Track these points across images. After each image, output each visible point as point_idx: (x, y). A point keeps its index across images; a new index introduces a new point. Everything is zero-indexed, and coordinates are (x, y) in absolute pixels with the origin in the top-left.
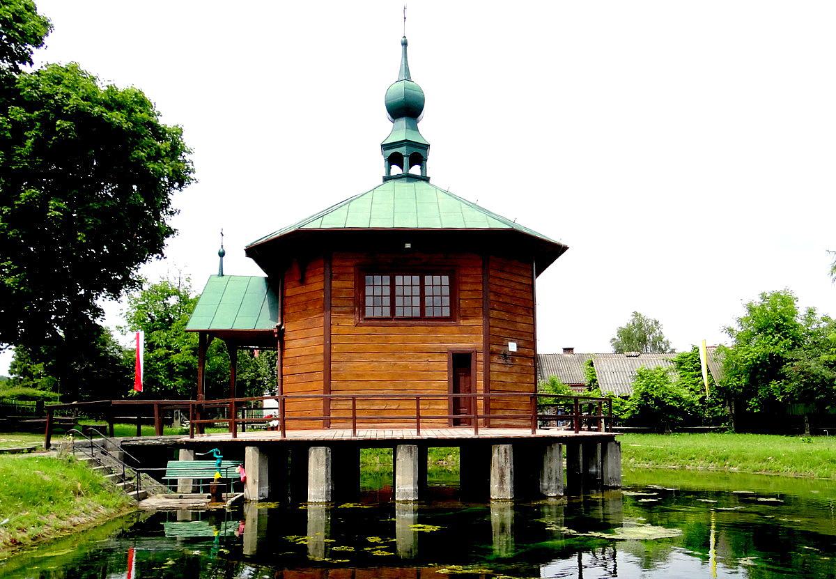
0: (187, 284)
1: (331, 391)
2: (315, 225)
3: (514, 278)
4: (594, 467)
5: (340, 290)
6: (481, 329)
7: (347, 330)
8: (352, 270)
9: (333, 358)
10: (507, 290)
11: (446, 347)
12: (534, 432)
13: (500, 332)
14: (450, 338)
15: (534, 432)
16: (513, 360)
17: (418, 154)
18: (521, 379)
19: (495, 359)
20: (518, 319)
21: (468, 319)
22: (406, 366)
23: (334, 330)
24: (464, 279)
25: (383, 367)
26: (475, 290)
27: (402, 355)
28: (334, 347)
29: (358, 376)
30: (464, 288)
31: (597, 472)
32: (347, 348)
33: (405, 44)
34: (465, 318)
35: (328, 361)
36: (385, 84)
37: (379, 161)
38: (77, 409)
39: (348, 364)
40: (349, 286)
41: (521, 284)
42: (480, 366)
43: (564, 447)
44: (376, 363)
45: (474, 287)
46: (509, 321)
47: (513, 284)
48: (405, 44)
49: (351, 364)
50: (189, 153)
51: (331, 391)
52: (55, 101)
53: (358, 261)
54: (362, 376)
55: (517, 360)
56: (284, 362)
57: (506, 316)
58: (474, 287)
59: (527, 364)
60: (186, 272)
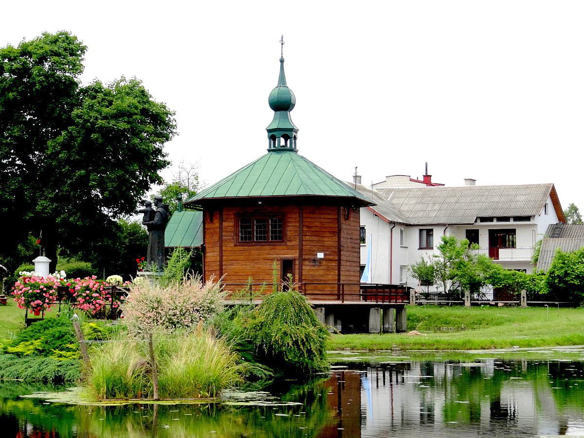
0: (195, 182)
1: (302, 280)
2: (210, 196)
3: (322, 216)
4: (387, 324)
5: (226, 227)
6: (298, 247)
7: (230, 249)
8: (233, 216)
9: (223, 263)
10: (317, 224)
11: (279, 257)
12: (343, 302)
13: (310, 248)
14: (282, 252)
15: (343, 302)
16: (320, 263)
17: (288, 134)
18: (327, 273)
19: (307, 263)
20: (325, 239)
21: (291, 242)
22: (259, 268)
23: (224, 248)
24: (290, 220)
25: (248, 267)
26: (295, 226)
27: (257, 261)
28: (224, 257)
29: (236, 272)
30: (289, 225)
31: (389, 327)
32: (231, 258)
33: (282, 61)
34: (290, 241)
35: (221, 261)
36: (269, 86)
37: (265, 142)
38: (16, 168)
39: (231, 266)
40: (232, 225)
41: (329, 219)
42: (297, 267)
43: (324, 308)
44: (244, 266)
45: (294, 224)
46: (318, 241)
47: (322, 220)
48: (282, 61)
49: (232, 266)
50: (174, 114)
51: (302, 280)
52: (90, 123)
53: (236, 211)
54: (238, 273)
55: (324, 263)
56: (206, 264)
57: (316, 239)
58: (294, 224)
59: (332, 264)
60: (192, 172)
